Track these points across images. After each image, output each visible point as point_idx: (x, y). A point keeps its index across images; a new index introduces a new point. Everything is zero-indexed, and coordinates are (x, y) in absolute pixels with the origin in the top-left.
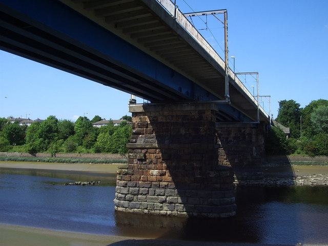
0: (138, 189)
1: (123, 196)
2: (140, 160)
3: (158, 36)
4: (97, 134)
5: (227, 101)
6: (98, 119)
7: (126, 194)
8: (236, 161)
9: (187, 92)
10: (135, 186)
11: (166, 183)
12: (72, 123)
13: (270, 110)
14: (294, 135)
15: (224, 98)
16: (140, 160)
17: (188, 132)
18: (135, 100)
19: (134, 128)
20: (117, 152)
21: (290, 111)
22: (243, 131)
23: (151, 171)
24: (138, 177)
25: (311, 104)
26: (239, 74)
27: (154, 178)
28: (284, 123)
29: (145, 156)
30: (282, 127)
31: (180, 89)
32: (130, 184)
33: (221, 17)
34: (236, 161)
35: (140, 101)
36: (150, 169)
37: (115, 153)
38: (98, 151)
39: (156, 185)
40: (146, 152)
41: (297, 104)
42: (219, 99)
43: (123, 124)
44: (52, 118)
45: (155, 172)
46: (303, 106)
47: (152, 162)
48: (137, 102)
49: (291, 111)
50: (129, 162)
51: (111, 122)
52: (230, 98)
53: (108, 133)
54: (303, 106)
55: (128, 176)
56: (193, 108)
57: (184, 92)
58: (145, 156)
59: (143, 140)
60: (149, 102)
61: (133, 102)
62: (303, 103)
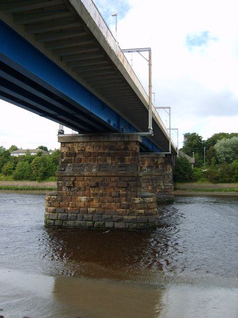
0: (66, 214)
1: (52, 221)
2: (69, 187)
3: (94, 65)
4: (16, 163)
5: (151, 133)
6: (14, 148)
7: (55, 220)
8: (149, 189)
9: (114, 124)
10: (64, 212)
11: (94, 209)
12: (58, 151)
13: (178, 142)
14: (198, 165)
15: (148, 130)
16: (69, 187)
17: (113, 162)
18: (63, 131)
19: (62, 157)
20: (35, 180)
21: (193, 140)
22: (156, 160)
23: (79, 198)
24: (67, 203)
25: (213, 137)
26: (159, 108)
27: (82, 204)
28: (190, 154)
29: (73, 183)
30: (188, 157)
31: (109, 121)
32: (59, 210)
33: (146, 54)
34: (149, 189)
35: (69, 131)
36: (78, 196)
37: (33, 180)
38: (18, 178)
39: (84, 211)
40: (75, 180)
41: (200, 137)
42: (139, 132)
43: (40, 154)
44: (194, 134)
45: (83, 199)
46: (205, 138)
47: (80, 189)
48: (65, 133)
49: (195, 142)
50: (58, 189)
51: (28, 151)
52: (153, 130)
53: (27, 162)
54: (205, 138)
55: (57, 202)
56: (119, 139)
57: (112, 124)
58: (73, 183)
59: (72, 168)
60: (77, 133)
61: (61, 132)
62: (205, 136)
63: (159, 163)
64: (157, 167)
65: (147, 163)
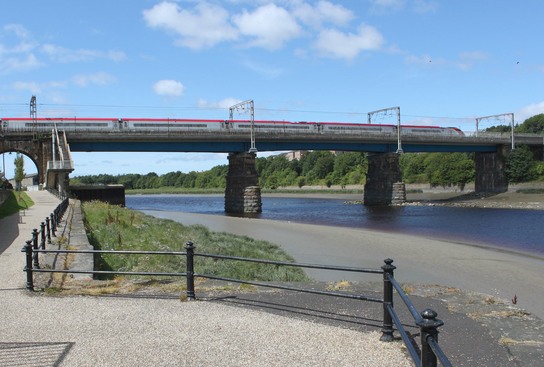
22: (388, 160)
63: (390, 163)
64: (389, 167)
65: (382, 163)
